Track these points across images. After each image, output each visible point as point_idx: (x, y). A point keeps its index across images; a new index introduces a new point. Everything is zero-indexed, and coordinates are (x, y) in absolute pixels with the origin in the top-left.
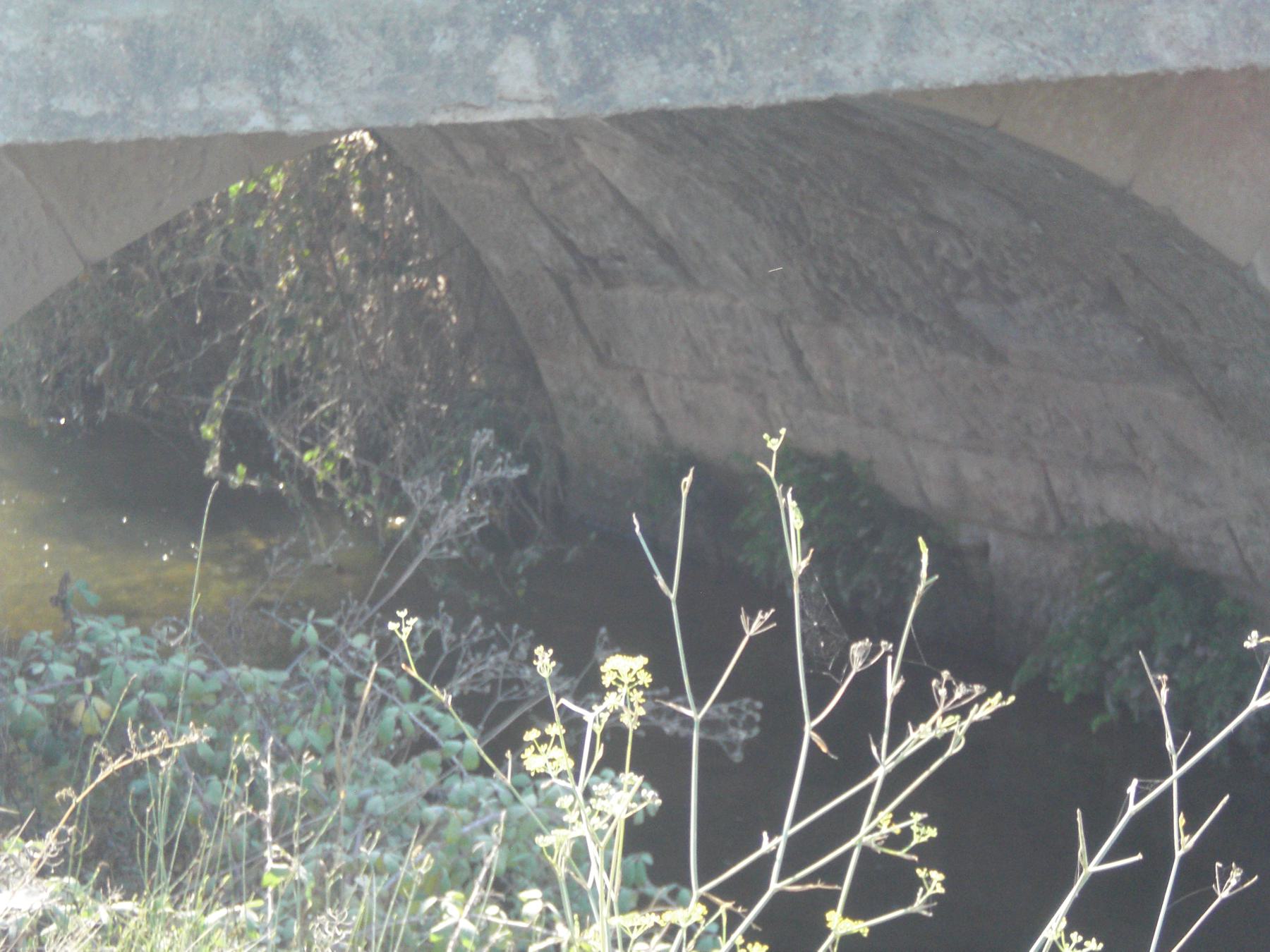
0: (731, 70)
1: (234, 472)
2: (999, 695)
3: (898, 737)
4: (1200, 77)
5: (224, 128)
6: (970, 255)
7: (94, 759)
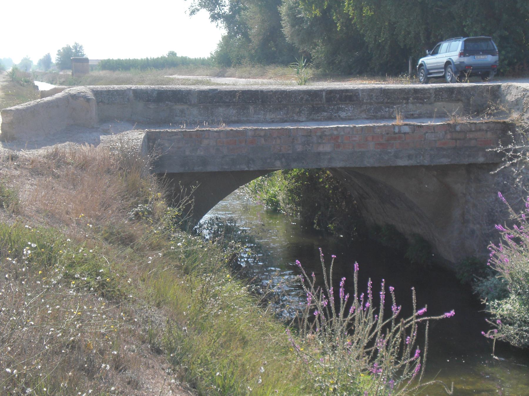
7: (344, 309)
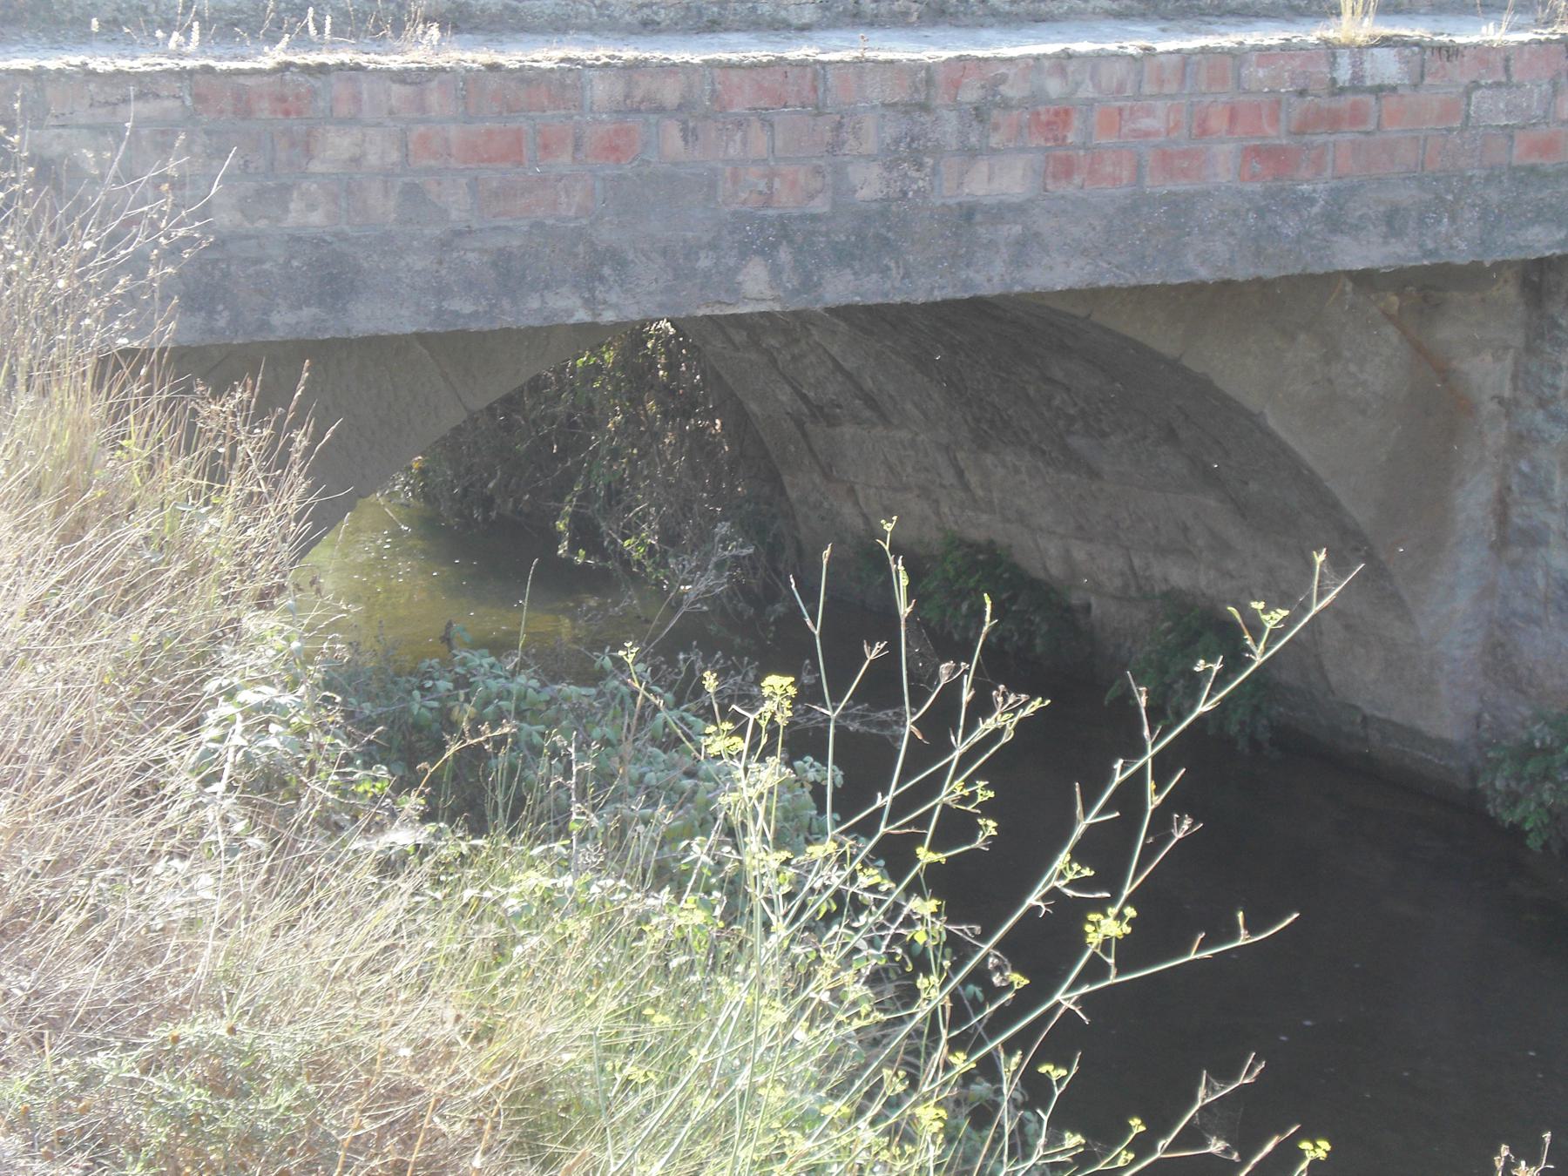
0: (903, 278)
1: (577, 555)
2: (1040, 699)
3: (970, 727)
4: (1227, 284)
5: (557, 321)
6: (1075, 405)
